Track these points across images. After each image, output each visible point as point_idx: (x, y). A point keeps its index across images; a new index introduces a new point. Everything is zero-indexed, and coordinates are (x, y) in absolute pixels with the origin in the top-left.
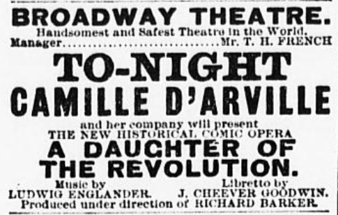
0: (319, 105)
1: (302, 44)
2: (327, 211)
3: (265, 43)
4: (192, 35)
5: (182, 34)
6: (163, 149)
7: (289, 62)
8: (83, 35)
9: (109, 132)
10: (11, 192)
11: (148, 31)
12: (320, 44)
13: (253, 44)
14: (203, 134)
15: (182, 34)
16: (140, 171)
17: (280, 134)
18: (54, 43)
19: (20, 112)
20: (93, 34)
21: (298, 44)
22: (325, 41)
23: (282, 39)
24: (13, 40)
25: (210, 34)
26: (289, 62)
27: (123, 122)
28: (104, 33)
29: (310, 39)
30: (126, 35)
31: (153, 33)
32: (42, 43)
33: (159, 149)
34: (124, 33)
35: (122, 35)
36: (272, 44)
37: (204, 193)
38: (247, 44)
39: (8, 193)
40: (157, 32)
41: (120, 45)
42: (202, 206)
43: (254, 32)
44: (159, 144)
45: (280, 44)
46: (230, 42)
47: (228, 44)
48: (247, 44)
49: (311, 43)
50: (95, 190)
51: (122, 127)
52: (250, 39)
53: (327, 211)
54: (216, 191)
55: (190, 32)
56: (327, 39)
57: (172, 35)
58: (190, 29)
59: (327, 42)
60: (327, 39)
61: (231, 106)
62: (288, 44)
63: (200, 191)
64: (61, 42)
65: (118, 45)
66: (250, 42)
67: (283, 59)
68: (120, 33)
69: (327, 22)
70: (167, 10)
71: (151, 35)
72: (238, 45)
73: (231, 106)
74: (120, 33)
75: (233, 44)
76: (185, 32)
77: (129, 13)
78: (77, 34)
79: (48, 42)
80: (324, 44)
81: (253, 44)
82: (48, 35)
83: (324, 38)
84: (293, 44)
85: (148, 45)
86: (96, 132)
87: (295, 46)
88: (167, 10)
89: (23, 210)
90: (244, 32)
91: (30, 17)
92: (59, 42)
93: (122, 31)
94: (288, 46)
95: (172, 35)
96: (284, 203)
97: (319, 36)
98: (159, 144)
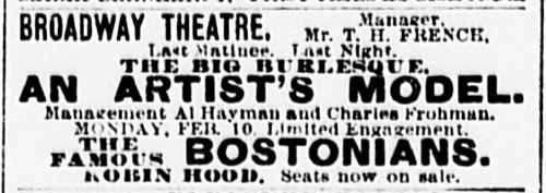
1: (438, 40)
11: (430, 175)
12: (466, 40)
16: (478, 94)
18: (115, 113)
21: (431, 40)
22: (473, 34)
24: (308, 30)
28: (324, 51)
30: (346, 180)
32: (428, 177)
34: (343, 178)
35: (389, 24)
37: (473, 34)
42: (424, 39)
45: (403, 39)
49: (451, 37)
50: (237, 57)
51: (434, 24)
52: (176, 62)
58: (346, 109)
62: (417, 40)
63: (466, 31)
64: (437, 18)
68: (477, 115)
69: (268, 37)
73: (41, 31)
74: (477, 115)
77: (67, 82)
78: (355, 178)
79: (417, 18)
82: (430, 181)
83: (473, 30)
84: (424, 39)
86: (438, 31)
91: (33, 26)
93: (75, 112)
96: (423, 35)
97: (465, 27)
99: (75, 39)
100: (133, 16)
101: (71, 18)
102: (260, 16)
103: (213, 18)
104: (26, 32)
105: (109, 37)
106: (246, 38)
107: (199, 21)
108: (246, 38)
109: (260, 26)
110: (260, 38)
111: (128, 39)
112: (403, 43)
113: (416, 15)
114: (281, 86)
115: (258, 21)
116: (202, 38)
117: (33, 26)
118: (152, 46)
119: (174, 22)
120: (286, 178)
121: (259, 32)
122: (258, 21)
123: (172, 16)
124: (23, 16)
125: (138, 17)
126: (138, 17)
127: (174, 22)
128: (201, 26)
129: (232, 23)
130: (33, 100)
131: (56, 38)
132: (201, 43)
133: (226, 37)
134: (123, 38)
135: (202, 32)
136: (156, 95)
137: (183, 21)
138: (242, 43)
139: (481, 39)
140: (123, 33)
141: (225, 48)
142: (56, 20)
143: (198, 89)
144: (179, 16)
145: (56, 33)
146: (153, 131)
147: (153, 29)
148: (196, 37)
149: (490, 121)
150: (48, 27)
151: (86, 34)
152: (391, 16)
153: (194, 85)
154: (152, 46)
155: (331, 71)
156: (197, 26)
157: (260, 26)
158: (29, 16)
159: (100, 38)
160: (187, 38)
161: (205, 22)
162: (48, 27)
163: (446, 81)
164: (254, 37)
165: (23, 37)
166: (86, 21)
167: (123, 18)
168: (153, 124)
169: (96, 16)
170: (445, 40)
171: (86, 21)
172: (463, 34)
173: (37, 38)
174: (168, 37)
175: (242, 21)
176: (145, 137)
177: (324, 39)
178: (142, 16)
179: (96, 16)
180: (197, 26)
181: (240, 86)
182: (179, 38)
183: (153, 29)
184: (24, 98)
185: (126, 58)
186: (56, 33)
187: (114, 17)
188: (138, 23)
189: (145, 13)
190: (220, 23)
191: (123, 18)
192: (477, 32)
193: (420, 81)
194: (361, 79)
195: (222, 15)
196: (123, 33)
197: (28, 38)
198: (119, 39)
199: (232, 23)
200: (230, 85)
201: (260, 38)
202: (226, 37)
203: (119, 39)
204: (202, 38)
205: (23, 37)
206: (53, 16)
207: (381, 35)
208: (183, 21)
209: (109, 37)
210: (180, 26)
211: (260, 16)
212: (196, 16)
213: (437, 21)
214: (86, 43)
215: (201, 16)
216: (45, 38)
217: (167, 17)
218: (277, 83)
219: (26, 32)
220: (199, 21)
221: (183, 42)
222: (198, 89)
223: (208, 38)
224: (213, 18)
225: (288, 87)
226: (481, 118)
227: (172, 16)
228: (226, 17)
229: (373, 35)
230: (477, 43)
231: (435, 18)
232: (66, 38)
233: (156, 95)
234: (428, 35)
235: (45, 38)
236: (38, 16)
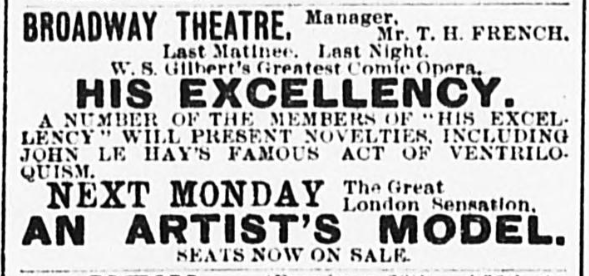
0: (80, 225)
1: (514, 38)
2: (567, 4)
3: (450, 36)
6: (278, 92)
7: (148, 191)
8: (372, 209)
9: (41, 126)
10: (25, 134)
14: (350, 68)
17: (496, 33)
22: (551, 33)
26: (148, 191)
27: (388, 12)
33: (273, 93)
39: (21, 136)
44: (272, 86)
51: (387, 21)
53: (567, 4)
54: (479, 30)
55: (364, 188)
58: (364, 182)
59: (555, 36)
60: (555, 30)
61: (261, 30)
67: (143, 188)
69: (289, 35)
70: (486, 81)
80: (551, 38)
83: (551, 28)
88: (486, 81)
89: (572, 241)
97: (543, 25)
98: (272, 86)
99: (83, 39)
100: (145, 15)
101: (79, 15)
102: (281, 13)
103: (231, 15)
104: (31, 32)
105: (120, 37)
106: (266, 37)
107: (217, 19)
108: (266, 37)
109: (281, 24)
110: (281, 38)
111: (139, 38)
112: (476, 42)
113: (368, 12)
114: (305, 226)
115: (279, 18)
116: (220, 38)
118: (167, 46)
119: (189, 20)
121: (280, 31)
122: (279, 18)
123: (188, 14)
124: (27, 16)
125: (150, 16)
126: (150, 16)
127: (189, 20)
128: (219, 25)
129: (251, 20)
130: (36, 242)
131: (63, 39)
132: (221, 43)
133: (246, 36)
134: (135, 38)
135: (220, 31)
136: (171, 236)
137: (199, 20)
138: (261, 42)
139: (559, 38)
140: (134, 32)
141: (245, 48)
142: (63, 19)
143: (217, 229)
144: (195, 14)
145: (63, 33)
146: (181, 155)
147: (167, 29)
148: (213, 37)
150: (54, 26)
151: (95, 32)
152: (341, 12)
153: (212, 225)
154: (167, 46)
155: (546, 158)
156: (214, 24)
157: (281, 24)
159: (110, 38)
160: (204, 37)
161: (222, 20)
162: (54, 26)
163: (430, 236)
164: (275, 37)
165: (27, 38)
166: (95, 19)
167: (135, 15)
170: (521, 38)
171: (95, 19)
172: (540, 32)
173: (43, 39)
174: (183, 37)
175: (261, 19)
176: (172, 163)
177: (398, 38)
178: (154, 14)
179: (106, 14)
180: (214, 24)
181: (318, 231)
182: (196, 37)
183: (167, 29)
184: (26, 241)
186: (63, 33)
187: (124, 15)
188: (150, 22)
190: (239, 20)
191: (135, 15)
192: (555, 30)
193: (425, 240)
194: (392, 217)
195: (241, 13)
196: (134, 32)
198: (130, 38)
199: (251, 20)
200: (255, 232)
201: (281, 38)
202: (246, 36)
203: (130, 38)
204: (220, 38)
206: (60, 15)
208: (199, 20)
209: (120, 37)
210: (196, 25)
211: (281, 13)
212: (213, 14)
213: (390, 19)
214: (94, 43)
215: (220, 13)
216: (51, 38)
217: (183, 15)
218: (301, 221)
220: (217, 19)
221: (200, 41)
222: (217, 229)
223: (226, 38)
224: (231, 15)
225: (312, 227)
227: (188, 14)
228: (245, 14)
230: (555, 42)
231: (388, 16)
232: (74, 39)
233: (171, 236)
234: (525, 154)
235: (51, 38)
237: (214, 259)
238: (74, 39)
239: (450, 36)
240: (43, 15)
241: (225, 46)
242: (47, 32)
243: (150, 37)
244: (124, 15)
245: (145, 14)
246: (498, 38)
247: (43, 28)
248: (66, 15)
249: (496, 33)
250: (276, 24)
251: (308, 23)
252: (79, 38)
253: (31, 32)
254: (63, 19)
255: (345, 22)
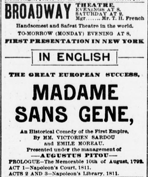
1: (54, 42)
3: (120, 19)
4: (112, 27)
5: (80, 27)
13: (116, 20)
15: (80, 27)
19: (22, 6)
20: (68, 132)
23: (77, 9)
25: (92, 27)
29: (54, 173)
31: (67, 26)
35: (90, 151)
36: (123, 20)
38: (114, 19)
40: (69, 26)
41: (93, 20)
42: (94, 15)
43: (112, 26)
46: (106, 18)
47: (105, 19)
48: (114, 19)
49: (33, 168)
56: (18, 25)
57: (107, 172)
65: (94, 20)
66: (115, 18)
71: (66, 27)
72: (110, 20)
73: (16, 14)
75: (107, 19)
76: (47, 162)
81: (116, 20)
82: (87, 151)
85: (94, 20)
87: (94, 16)
90: (107, 26)
91: (12, 11)
92: (84, 18)
94: (92, 16)
95: (76, 27)
97: (118, 72)
99: (34, 17)
101: (31, 6)
104: (8, 14)
105: (51, 17)
111: (61, 17)
112: (28, 152)
114: (131, 124)
117: (12, 11)
120: (62, 27)
125: (67, 6)
126: (67, 6)
142: (23, 7)
145: (23, 15)
149: (122, 20)
150: (19, 11)
155: (94, 154)
158: (10, 5)
162: (19, 11)
165: (7, 17)
167: (59, 6)
168: (109, 156)
169: (45, 6)
171: (39, 7)
173: (14, 18)
178: (70, 5)
179: (45, 6)
185: (52, 72)
186: (23, 15)
189: (71, 4)
191: (59, 6)
197: (10, 17)
198: (57, 17)
203: (57, 17)
205: (7, 17)
207: (121, 18)
216: (17, 17)
219: (8, 15)
226: (103, 27)
229: (119, 18)
232: (29, 17)
234: (95, 14)
236: (14, 5)
237: (81, 15)
238: (29, 17)
239: (120, 19)
240: (14, 5)
241: (79, 17)
242: (16, 14)
243: (67, 17)
244: (53, 6)
245: (65, 5)
246: (90, 145)
247: (14, 11)
248: (40, 5)
249: (102, 137)
250: (121, 114)
251: (79, 145)
252: (31, 17)
253: (8, 14)
254: (23, 7)
255: (85, 151)
